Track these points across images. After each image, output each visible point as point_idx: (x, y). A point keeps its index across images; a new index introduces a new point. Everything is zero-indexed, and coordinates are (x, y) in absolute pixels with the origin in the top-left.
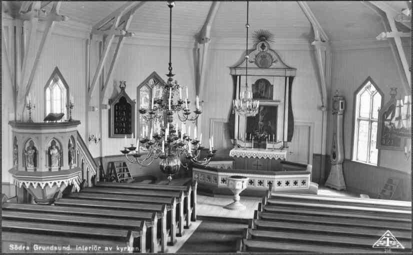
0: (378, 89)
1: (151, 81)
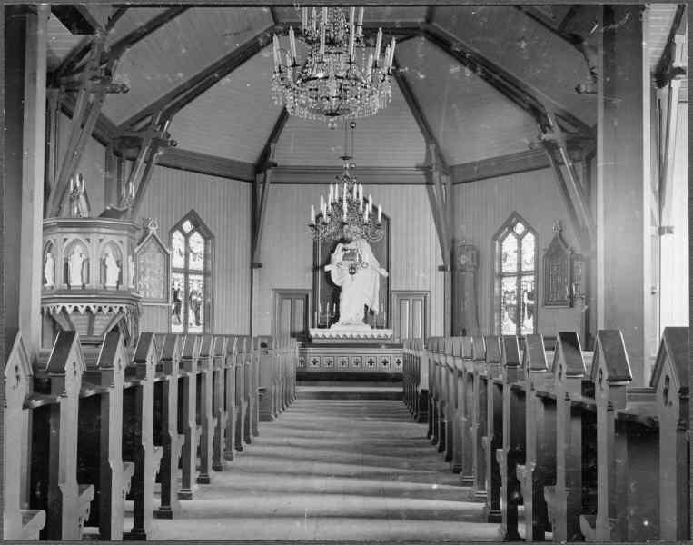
0: (529, 228)
1: (187, 226)
